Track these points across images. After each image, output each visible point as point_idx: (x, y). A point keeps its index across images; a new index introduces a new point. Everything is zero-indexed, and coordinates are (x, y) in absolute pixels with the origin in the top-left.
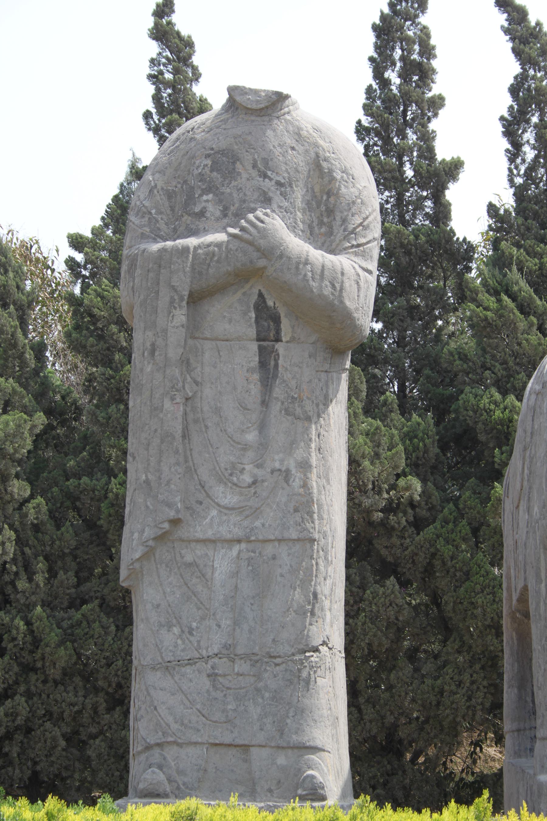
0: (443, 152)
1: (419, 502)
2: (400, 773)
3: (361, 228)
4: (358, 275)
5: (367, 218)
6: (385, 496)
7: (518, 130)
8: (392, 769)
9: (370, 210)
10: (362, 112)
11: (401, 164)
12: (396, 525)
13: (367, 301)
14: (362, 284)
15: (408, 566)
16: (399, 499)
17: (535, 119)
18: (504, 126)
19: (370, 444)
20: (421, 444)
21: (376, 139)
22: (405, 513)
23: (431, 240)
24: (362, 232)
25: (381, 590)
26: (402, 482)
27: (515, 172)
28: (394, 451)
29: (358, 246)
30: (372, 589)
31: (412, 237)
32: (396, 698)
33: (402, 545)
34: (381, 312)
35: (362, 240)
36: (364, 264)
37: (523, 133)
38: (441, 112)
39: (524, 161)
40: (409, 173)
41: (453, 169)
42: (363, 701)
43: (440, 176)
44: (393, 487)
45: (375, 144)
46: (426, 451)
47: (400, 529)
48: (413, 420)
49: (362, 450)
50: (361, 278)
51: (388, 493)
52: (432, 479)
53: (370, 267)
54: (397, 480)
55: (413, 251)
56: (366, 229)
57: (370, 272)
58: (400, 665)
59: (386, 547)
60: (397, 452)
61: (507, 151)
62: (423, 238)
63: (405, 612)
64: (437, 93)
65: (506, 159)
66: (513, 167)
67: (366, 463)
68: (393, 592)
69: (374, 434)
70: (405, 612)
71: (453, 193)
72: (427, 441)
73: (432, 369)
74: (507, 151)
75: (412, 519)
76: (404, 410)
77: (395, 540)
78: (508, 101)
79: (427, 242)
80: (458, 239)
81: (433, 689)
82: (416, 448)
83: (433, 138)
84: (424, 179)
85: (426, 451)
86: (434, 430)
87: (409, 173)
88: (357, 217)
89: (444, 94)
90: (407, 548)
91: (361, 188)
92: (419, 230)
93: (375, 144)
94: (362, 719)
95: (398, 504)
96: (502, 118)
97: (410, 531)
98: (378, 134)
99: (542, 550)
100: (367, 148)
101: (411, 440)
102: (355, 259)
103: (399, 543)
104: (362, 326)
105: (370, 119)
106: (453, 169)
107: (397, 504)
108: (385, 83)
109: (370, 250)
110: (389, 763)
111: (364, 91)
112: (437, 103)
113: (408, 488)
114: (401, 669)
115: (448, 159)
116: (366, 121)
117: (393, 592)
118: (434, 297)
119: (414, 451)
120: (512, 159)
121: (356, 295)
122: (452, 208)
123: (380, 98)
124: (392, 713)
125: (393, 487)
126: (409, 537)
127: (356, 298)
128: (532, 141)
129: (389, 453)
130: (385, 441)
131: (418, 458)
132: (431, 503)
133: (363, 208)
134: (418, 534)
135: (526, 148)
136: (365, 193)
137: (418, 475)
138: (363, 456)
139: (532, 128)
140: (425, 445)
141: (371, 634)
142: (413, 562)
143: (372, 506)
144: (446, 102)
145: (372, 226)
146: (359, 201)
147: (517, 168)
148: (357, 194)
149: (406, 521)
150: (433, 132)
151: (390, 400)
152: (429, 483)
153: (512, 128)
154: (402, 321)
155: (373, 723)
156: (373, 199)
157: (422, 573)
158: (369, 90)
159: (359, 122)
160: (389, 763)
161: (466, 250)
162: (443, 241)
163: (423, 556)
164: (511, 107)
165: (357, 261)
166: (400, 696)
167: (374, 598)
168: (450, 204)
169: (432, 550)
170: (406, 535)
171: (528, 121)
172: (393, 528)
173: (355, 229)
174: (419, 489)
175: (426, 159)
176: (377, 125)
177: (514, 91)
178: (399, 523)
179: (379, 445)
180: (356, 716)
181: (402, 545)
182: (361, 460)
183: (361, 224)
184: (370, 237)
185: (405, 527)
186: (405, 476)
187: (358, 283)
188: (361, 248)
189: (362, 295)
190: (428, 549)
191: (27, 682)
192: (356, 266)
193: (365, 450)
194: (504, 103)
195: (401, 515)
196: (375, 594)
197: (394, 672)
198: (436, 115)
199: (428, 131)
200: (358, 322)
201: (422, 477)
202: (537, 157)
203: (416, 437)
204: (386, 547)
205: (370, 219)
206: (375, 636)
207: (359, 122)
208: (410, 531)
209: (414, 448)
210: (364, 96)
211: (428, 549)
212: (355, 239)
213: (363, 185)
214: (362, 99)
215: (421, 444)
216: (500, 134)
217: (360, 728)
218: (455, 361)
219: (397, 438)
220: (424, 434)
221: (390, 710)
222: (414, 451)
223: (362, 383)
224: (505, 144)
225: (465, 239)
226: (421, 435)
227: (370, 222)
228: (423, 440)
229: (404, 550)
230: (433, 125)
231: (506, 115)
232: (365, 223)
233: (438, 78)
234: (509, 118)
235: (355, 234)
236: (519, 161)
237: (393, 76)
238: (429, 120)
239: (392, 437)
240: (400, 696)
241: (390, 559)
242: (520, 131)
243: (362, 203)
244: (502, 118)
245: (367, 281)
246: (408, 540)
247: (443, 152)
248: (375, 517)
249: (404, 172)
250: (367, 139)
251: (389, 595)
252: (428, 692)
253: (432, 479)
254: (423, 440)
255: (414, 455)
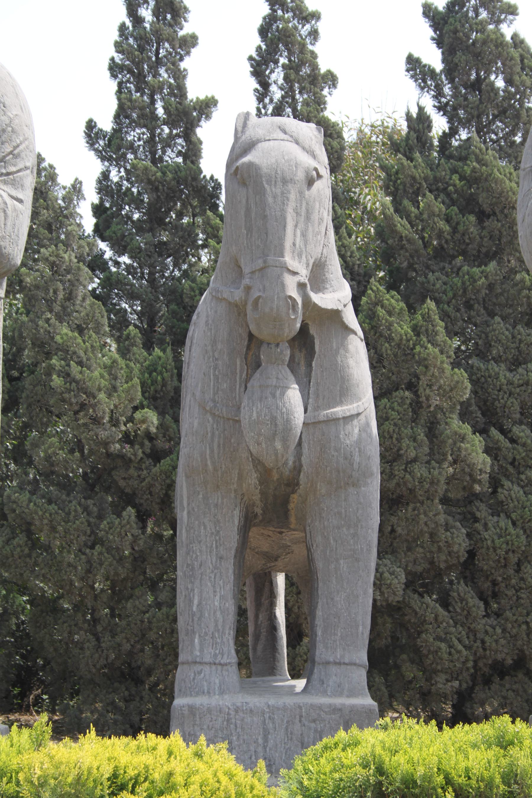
0: (195, 91)
1: (156, 434)
2: (138, 699)
3: (11, 156)
4: (5, 203)
5: (18, 146)
6: (123, 428)
7: (266, 70)
8: (130, 695)
9: (21, 139)
10: (114, 49)
11: (153, 102)
12: (133, 457)
13: (16, 230)
14: (9, 212)
15: (145, 497)
16: (135, 432)
17: (283, 60)
18: (252, 66)
19: (107, 376)
20: (159, 378)
21: (128, 76)
22: (142, 445)
23: (179, 177)
24: (12, 161)
25: (117, 521)
26: (138, 415)
27: (263, 111)
28: (130, 384)
29: (8, 174)
30: (108, 520)
31: (159, 174)
32: (132, 625)
33: (139, 476)
34: (129, 247)
35: (13, 169)
36: (14, 193)
37: (270, 73)
38: (193, 50)
39: (271, 100)
40: (160, 112)
41: (206, 107)
42: (101, 629)
43: (188, 116)
44: (131, 419)
45: (128, 81)
46: (164, 385)
47: (137, 461)
48: (154, 354)
49: (97, 383)
50: (9, 206)
51: (125, 425)
52: (171, 412)
53: (20, 196)
54: (133, 413)
55: (160, 187)
56: (16, 158)
57: (20, 201)
58: (137, 594)
59: (124, 479)
60: (133, 385)
61: (256, 90)
62: (170, 176)
63: (141, 542)
64: (190, 32)
65: (254, 99)
66: (261, 106)
67: (102, 396)
68: (128, 523)
69: (111, 367)
70: (141, 542)
71: (204, 131)
72: (165, 375)
73: (178, 304)
74: (256, 90)
75: (148, 451)
76: (148, 346)
77: (132, 472)
78: (257, 41)
79: (174, 179)
80: (205, 177)
81: (168, 617)
82: (154, 382)
83: (185, 77)
84: (173, 117)
85: (164, 385)
86: (173, 364)
87: (160, 112)
88: (7, 145)
89: (197, 33)
90: (144, 479)
91: (12, 116)
92: (166, 167)
93: (128, 81)
94: (100, 647)
95: (136, 435)
96: (251, 58)
97: (147, 462)
98: (130, 71)
99: (184, 478)
100: (120, 84)
101: (150, 374)
102: (5, 187)
103: (136, 474)
104: (9, 254)
105: (121, 56)
106: (206, 107)
107: (134, 436)
108: (137, 20)
109: (21, 178)
110: (127, 690)
111: (117, 28)
112: (190, 42)
113: (144, 421)
114: (138, 598)
115: (202, 97)
116: (118, 58)
117: (128, 523)
118: (181, 233)
119: (152, 385)
120: (260, 99)
121: (2, 223)
122: (203, 146)
123: (132, 36)
124: (128, 641)
125: (131, 419)
126: (147, 468)
127: (3, 226)
128: (281, 81)
129: (125, 386)
130: (122, 373)
131: (156, 391)
132: (169, 436)
133: (14, 136)
134: (155, 466)
135: (273, 88)
136: (16, 121)
137: (156, 408)
138: (100, 390)
139: (280, 69)
140: (163, 379)
141: (106, 563)
142: (150, 493)
143: (108, 438)
144: (199, 41)
145: (23, 155)
146: (10, 129)
147: (265, 107)
148: (8, 122)
149: (143, 452)
150: (185, 70)
151: (132, 334)
152: (167, 416)
153: (260, 68)
154: (150, 257)
155: (111, 651)
156: (25, 128)
157: (158, 503)
158: (122, 28)
159: (112, 59)
160: (127, 690)
161: (213, 188)
162: (190, 178)
163: (159, 488)
164: (259, 48)
165: (6, 189)
166: (136, 624)
167: (110, 528)
168: (201, 143)
169: (168, 481)
170: (143, 467)
171: (276, 62)
172: (130, 460)
173: (4, 157)
174: (156, 422)
175: (175, 96)
176: (128, 62)
177: (263, 32)
178: (135, 455)
179: (116, 378)
180: (93, 644)
181: (139, 476)
182: (97, 393)
183: (11, 153)
184: (21, 166)
185: (142, 458)
186: (143, 408)
187: (5, 211)
188: (11, 177)
189: (9, 223)
190: (164, 481)
191: (507, 620)
192: (5, 195)
193: (100, 383)
194: (253, 42)
195: (137, 447)
196: (111, 525)
197: (131, 601)
198: (188, 53)
199: (179, 70)
200: (4, 251)
201: (161, 410)
202: (283, 97)
203: (155, 370)
204: (124, 479)
205: (21, 147)
206: (110, 565)
207: (112, 59)
208: (147, 462)
209: (152, 381)
210: (117, 33)
211: (164, 481)
212: (5, 168)
213: (15, 113)
214: (115, 36)
215: (159, 378)
216: (249, 74)
217: (97, 655)
218: (195, 296)
219: (136, 371)
220: (163, 367)
221: (126, 638)
222: (152, 385)
223: (102, 317)
224: (253, 84)
225: (212, 177)
226: (160, 368)
227: (22, 151)
228: (161, 373)
229: (141, 482)
230: (183, 65)
231: (254, 55)
232: (16, 152)
233: (190, 16)
234: (257, 58)
235: (5, 162)
236: (267, 100)
237: (146, 13)
238: (181, 59)
239: (131, 370)
240: (136, 624)
241: (128, 490)
242: (267, 72)
243: (13, 131)
244: (251, 58)
245: (15, 210)
246: (145, 472)
247: (195, 91)
248: (112, 449)
249: (156, 109)
250: (120, 76)
251: (124, 526)
252: (163, 621)
253: (171, 412)
254: (161, 373)
255: (152, 388)
